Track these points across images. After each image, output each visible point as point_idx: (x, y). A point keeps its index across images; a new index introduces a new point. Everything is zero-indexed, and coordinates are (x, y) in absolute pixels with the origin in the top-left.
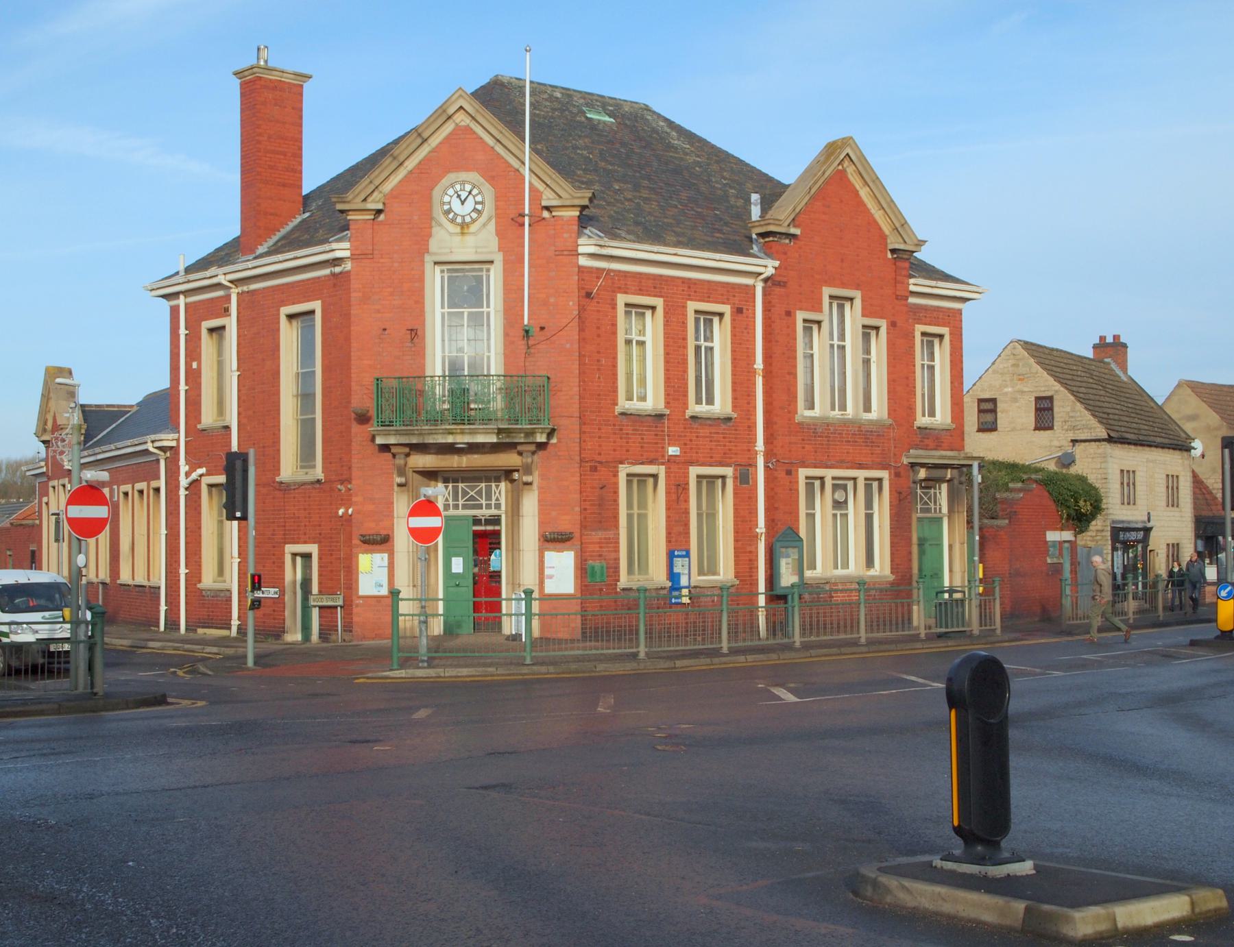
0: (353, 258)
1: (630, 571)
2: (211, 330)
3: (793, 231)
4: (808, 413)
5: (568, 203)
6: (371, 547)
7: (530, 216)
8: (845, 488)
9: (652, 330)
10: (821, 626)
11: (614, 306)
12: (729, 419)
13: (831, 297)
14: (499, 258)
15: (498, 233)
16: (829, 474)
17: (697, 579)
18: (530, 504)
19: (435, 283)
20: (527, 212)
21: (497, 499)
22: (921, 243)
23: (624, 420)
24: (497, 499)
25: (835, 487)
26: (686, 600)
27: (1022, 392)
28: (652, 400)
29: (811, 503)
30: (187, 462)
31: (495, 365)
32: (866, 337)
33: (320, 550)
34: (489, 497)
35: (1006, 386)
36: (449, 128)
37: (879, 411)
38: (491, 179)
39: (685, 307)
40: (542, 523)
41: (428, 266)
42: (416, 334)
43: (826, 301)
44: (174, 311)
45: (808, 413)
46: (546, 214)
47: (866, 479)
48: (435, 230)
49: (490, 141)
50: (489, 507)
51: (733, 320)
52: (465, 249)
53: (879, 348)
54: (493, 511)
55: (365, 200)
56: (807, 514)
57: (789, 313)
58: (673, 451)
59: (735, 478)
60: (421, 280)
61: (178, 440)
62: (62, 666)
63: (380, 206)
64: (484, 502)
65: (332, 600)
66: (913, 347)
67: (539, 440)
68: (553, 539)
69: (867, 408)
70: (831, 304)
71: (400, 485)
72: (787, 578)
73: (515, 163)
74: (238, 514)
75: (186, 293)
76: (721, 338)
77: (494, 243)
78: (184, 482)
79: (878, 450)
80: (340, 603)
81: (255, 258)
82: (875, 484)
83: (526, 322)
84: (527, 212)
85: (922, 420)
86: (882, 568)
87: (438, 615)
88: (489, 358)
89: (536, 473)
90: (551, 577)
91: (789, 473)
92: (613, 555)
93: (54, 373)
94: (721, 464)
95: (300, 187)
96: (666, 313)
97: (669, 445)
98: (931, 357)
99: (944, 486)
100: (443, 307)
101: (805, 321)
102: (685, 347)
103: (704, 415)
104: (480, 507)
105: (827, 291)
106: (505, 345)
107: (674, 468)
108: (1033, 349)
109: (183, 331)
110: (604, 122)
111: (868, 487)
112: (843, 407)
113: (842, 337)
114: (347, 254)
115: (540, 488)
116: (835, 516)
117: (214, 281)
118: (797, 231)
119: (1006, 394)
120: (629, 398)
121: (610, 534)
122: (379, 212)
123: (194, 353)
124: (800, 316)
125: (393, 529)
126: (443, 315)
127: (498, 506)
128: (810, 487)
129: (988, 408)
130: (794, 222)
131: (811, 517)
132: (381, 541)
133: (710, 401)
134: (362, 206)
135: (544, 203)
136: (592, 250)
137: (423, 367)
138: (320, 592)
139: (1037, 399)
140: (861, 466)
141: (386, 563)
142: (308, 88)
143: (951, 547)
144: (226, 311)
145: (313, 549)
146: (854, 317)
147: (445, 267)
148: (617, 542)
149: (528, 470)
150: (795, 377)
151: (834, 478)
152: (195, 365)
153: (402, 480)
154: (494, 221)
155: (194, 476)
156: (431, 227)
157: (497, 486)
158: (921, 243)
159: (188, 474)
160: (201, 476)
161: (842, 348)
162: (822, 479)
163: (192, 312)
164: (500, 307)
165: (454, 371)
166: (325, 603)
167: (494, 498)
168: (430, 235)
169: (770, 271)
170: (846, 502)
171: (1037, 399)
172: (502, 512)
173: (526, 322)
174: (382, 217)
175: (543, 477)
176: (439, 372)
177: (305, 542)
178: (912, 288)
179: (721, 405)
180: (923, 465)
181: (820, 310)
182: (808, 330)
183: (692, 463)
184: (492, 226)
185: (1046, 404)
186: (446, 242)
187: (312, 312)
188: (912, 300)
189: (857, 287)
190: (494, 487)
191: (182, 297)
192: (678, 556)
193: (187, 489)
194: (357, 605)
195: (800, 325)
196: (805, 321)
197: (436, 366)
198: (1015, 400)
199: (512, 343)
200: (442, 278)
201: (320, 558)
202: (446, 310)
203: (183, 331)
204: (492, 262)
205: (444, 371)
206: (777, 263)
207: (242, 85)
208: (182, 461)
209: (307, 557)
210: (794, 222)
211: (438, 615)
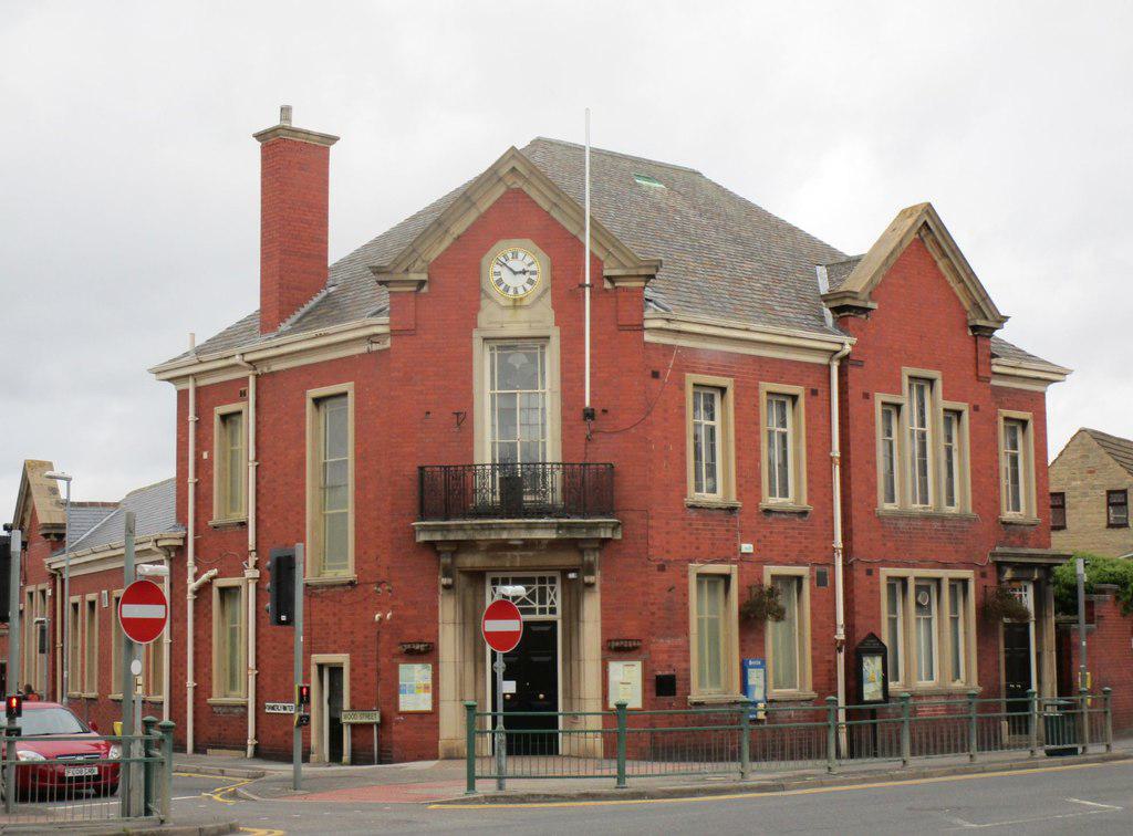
0: (394, 333)
1: (701, 684)
2: (224, 418)
3: (870, 305)
4: (888, 506)
5: (633, 272)
6: (575, 656)
7: (591, 286)
8: (927, 589)
9: (724, 419)
10: (924, 746)
11: (682, 387)
12: (804, 513)
13: (911, 377)
14: (555, 333)
15: (555, 306)
16: (912, 573)
17: (775, 693)
18: (592, 607)
19: (484, 364)
20: (588, 282)
21: (552, 603)
22: (1002, 320)
23: (693, 514)
24: (552, 603)
25: (918, 589)
26: (761, 715)
27: (1093, 488)
28: (721, 492)
29: (893, 609)
30: (196, 563)
31: (552, 452)
32: (948, 421)
33: (352, 661)
34: (542, 601)
35: (1075, 479)
36: (500, 191)
37: (963, 503)
38: (545, 245)
39: (756, 388)
40: (605, 630)
41: (477, 343)
42: (463, 419)
43: (906, 381)
44: (183, 395)
45: (888, 506)
46: (607, 285)
47: (951, 579)
48: (484, 303)
49: (546, 207)
50: (543, 611)
51: (807, 403)
52: (516, 326)
53: (963, 434)
54: (548, 617)
55: (407, 270)
56: (890, 619)
57: (866, 396)
58: (747, 548)
59: (812, 579)
60: (469, 357)
61: (185, 539)
62: (84, 791)
63: (424, 277)
64: (536, 605)
65: (368, 717)
66: (995, 433)
67: (603, 536)
68: (617, 649)
69: (951, 502)
70: (910, 385)
71: (446, 587)
72: (871, 690)
73: (573, 230)
74: (284, 618)
75: (195, 376)
76: (795, 425)
77: (550, 316)
78: (192, 585)
79: (963, 547)
80: (377, 719)
81: (278, 336)
82: (899, 585)
83: (587, 403)
84: (588, 282)
85: (1008, 515)
86: (968, 680)
87: (562, 732)
88: (544, 443)
89: (598, 573)
90: (426, 688)
91: (869, 572)
92: (684, 665)
93: (29, 468)
94: (797, 563)
95: (326, 259)
96: (737, 395)
97: (742, 542)
98: (1014, 446)
99: (1031, 589)
100: (493, 388)
101: (884, 404)
102: (758, 433)
103: (777, 508)
104: (532, 611)
105: (907, 371)
106: (563, 430)
107: (747, 567)
108: (1101, 439)
109: (192, 417)
110: (655, 190)
111: (953, 588)
112: (925, 500)
113: (923, 424)
114: (385, 330)
115: (604, 590)
116: (918, 619)
117: (231, 361)
118: (874, 305)
119: (1075, 489)
120: (698, 488)
121: (680, 641)
122: (421, 283)
123: (203, 442)
124: (879, 398)
125: (437, 637)
126: (493, 396)
127: (553, 611)
128: (891, 587)
129: (1058, 502)
130: (872, 296)
131: (893, 622)
132: (425, 652)
133: (785, 494)
134: (405, 277)
135: (606, 273)
136: (659, 324)
137: (471, 454)
138: (353, 708)
139: (1109, 493)
140: (945, 566)
141: (755, 670)
142: (333, 149)
143: (1039, 655)
144: (244, 394)
145: (342, 658)
146: (937, 402)
147: (494, 344)
148: (687, 651)
149: (590, 570)
150: (875, 467)
151: (917, 579)
152: (205, 455)
153: (450, 581)
154: (549, 292)
155: (204, 577)
156: (479, 300)
157: (552, 589)
158: (1002, 320)
159: (196, 577)
160: (212, 578)
161: (923, 435)
162: (904, 580)
163: (205, 400)
164: (557, 387)
165: (505, 465)
166: (359, 720)
167: (548, 602)
168: (478, 308)
169: (848, 349)
170: (929, 605)
171: (1109, 493)
172: (558, 617)
173: (587, 403)
174: (425, 289)
175: (605, 577)
176: (488, 460)
177: (335, 652)
178: (996, 369)
179: (796, 496)
180: (1009, 564)
181: (900, 392)
182: (887, 416)
183: (765, 562)
184: (548, 300)
185: (1117, 499)
186: (494, 319)
187: (345, 394)
188: (995, 382)
189: (937, 367)
190: (548, 590)
191: (191, 379)
192: (753, 667)
193: (196, 593)
194: (397, 722)
195: (879, 409)
196: (884, 404)
197: (485, 451)
198: (1085, 494)
199: (571, 427)
200: (492, 355)
201: (352, 670)
202: (497, 391)
203: (192, 417)
204: (548, 338)
205: (494, 459)
206: (854, 340)
207: (263, 148)
208: (190, 561)
209: (336, 671)
210: (872, 296)
211: (486, 732)
